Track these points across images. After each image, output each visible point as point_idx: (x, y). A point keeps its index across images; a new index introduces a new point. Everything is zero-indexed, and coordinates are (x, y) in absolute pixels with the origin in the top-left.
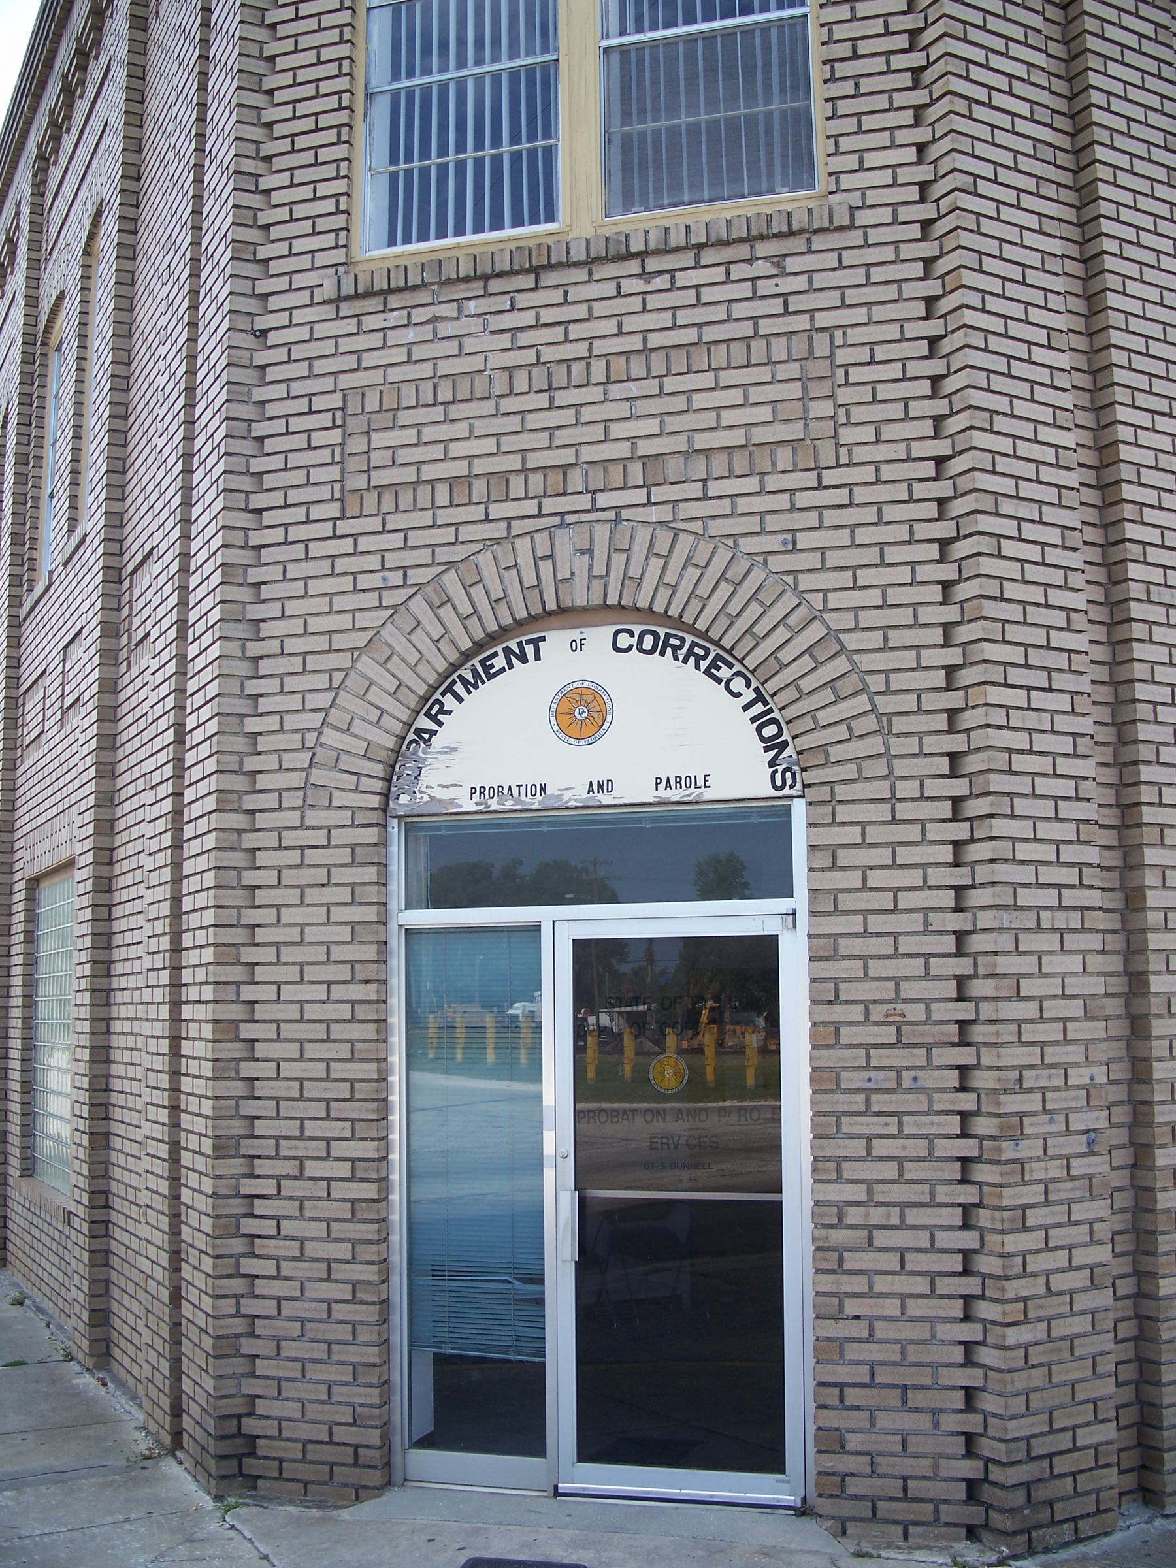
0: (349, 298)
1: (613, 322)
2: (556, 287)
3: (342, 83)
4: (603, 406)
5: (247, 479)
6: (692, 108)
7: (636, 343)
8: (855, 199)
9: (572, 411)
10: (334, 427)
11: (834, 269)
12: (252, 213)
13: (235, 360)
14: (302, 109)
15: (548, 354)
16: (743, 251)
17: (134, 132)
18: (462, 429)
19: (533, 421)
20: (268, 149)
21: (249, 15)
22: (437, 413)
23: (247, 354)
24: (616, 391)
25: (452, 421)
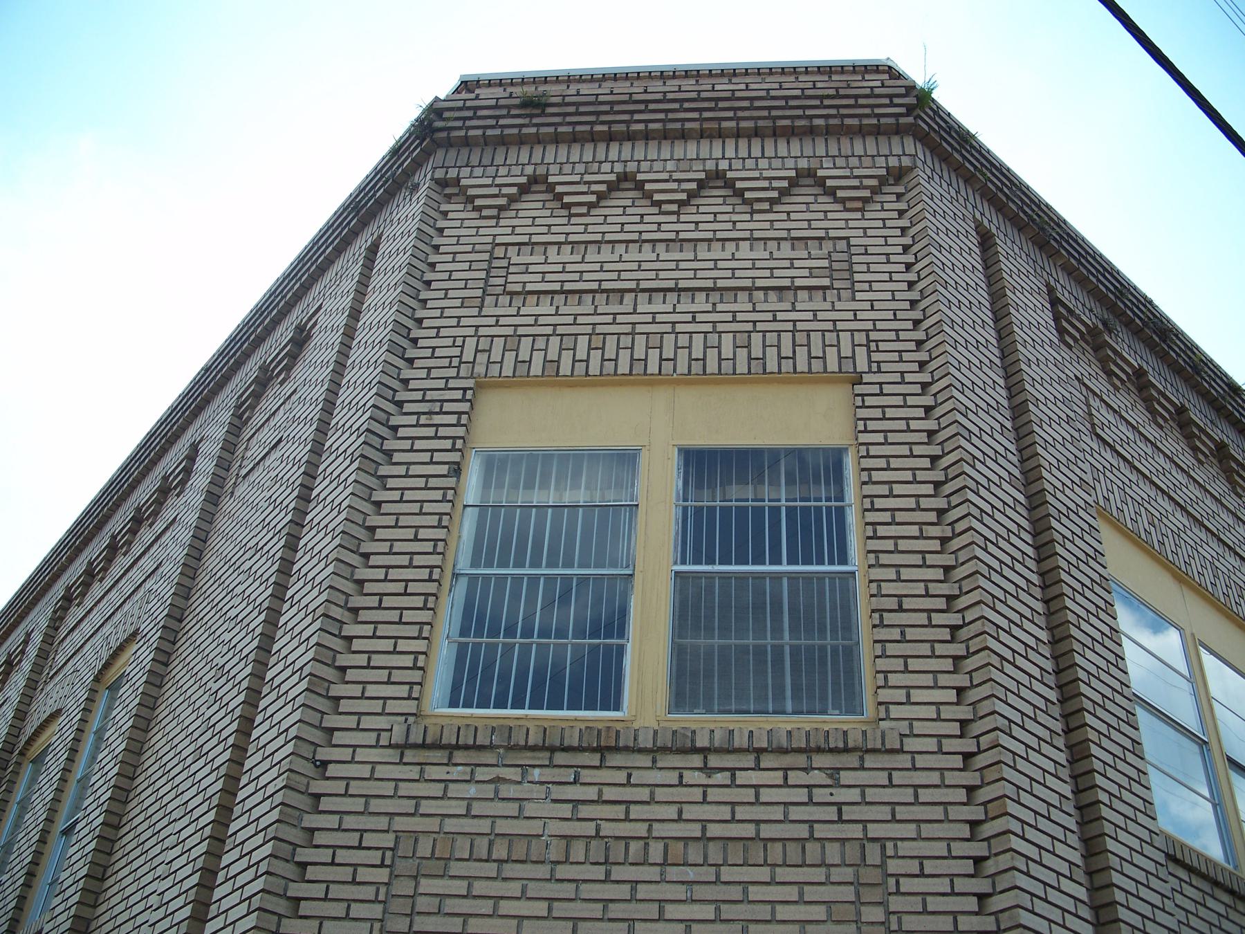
0: (415, 746)
1: (674, 808)
2: (619, 768)
3: (435, 560)
4: (659, 886)
5: (283, 902)
6: (760, 632)
7: (695, 830)
8: (904, 727)
9: (628, 887)
10: (382, 865)
11: (884, 786)
12: (332, 653)
13: (292, 784)
14: (393, 574)
15: (608, 829)
16: (801, 760)
17: (187, 582)
18: (514, 889)
19: (587, 891)
20: (356, 601)
21: (359, 490)
22: (490, 869)
23: (305, 780)
24: (673, 873)
25: (505, 879)
